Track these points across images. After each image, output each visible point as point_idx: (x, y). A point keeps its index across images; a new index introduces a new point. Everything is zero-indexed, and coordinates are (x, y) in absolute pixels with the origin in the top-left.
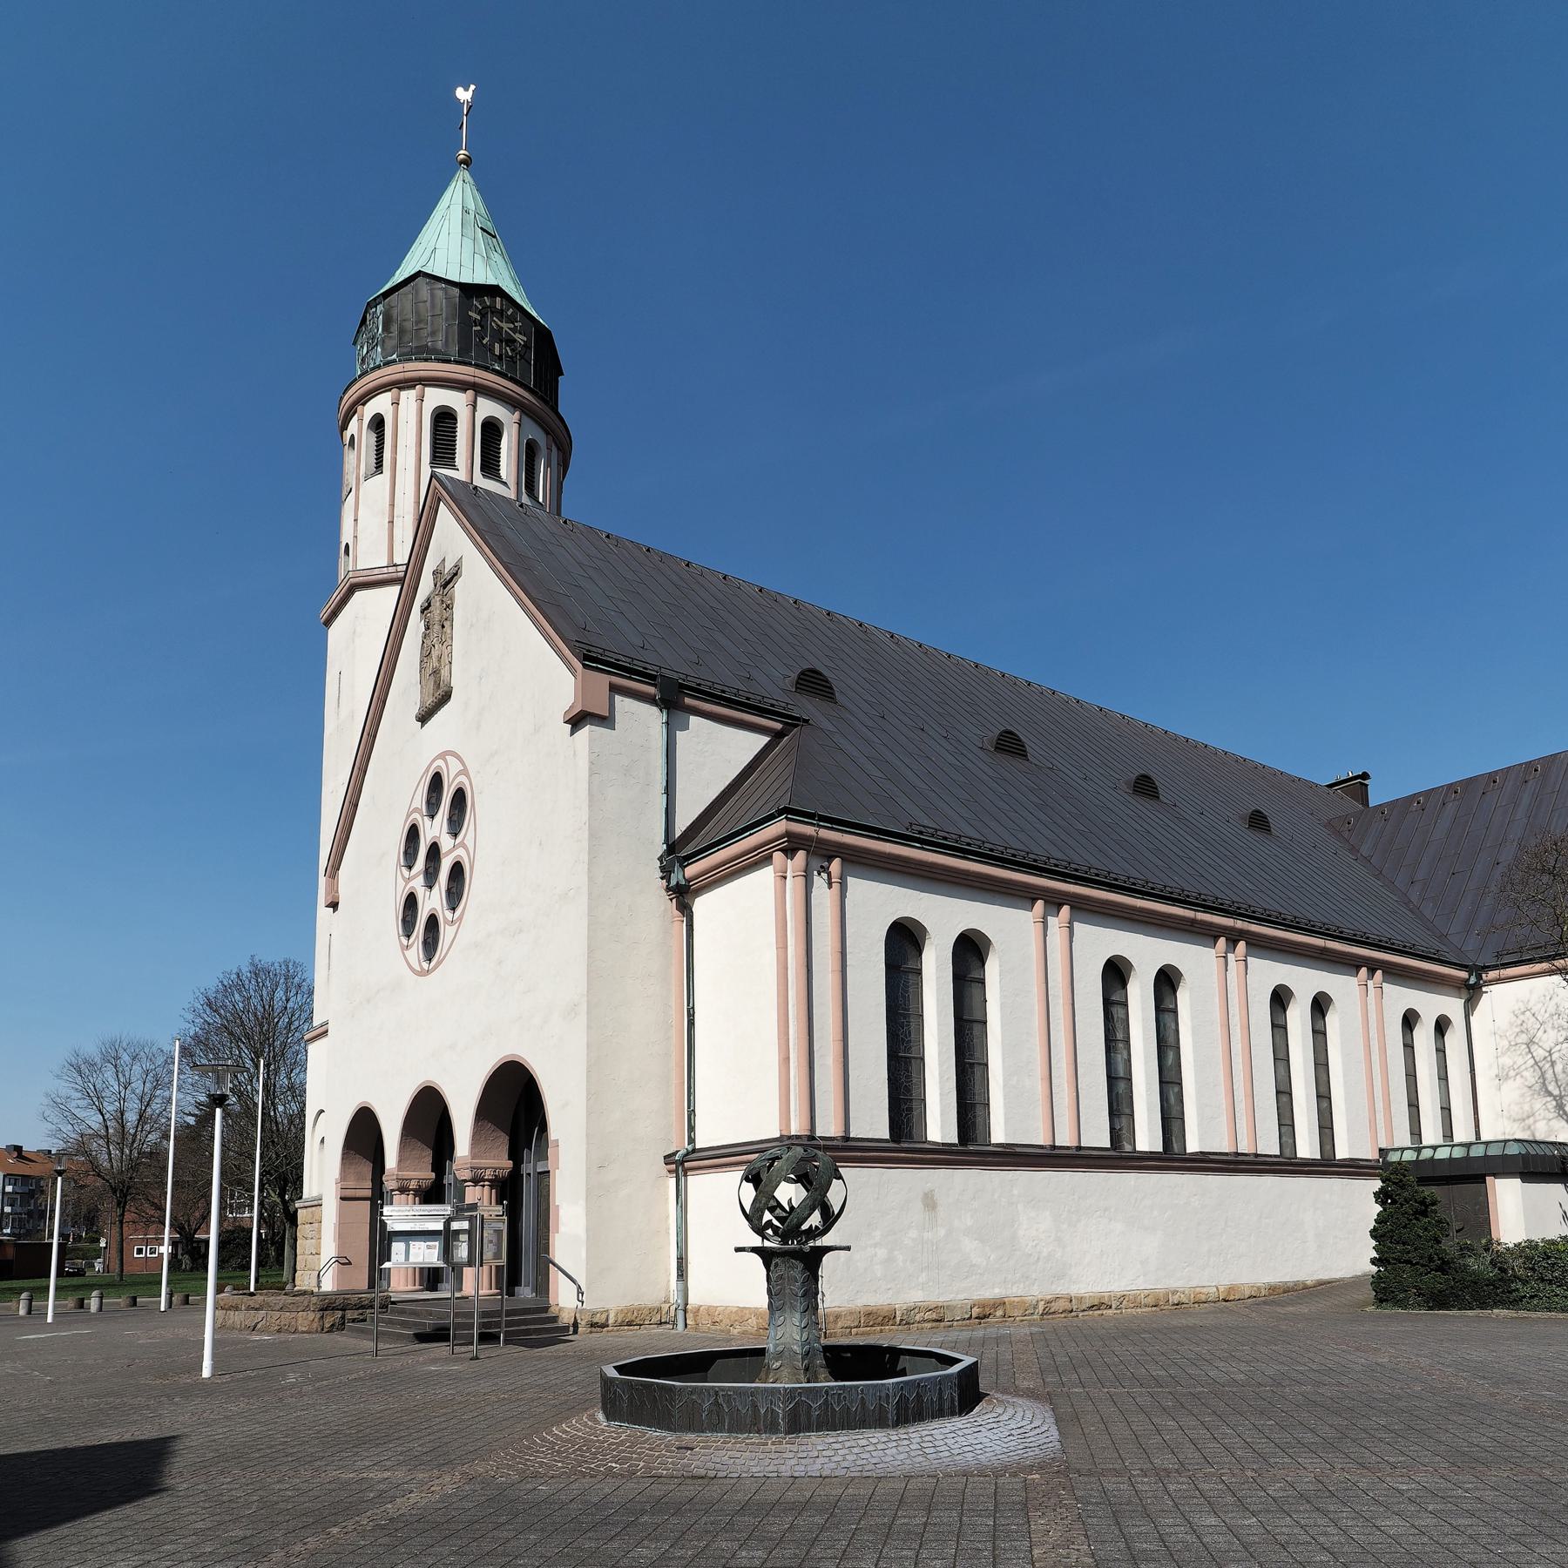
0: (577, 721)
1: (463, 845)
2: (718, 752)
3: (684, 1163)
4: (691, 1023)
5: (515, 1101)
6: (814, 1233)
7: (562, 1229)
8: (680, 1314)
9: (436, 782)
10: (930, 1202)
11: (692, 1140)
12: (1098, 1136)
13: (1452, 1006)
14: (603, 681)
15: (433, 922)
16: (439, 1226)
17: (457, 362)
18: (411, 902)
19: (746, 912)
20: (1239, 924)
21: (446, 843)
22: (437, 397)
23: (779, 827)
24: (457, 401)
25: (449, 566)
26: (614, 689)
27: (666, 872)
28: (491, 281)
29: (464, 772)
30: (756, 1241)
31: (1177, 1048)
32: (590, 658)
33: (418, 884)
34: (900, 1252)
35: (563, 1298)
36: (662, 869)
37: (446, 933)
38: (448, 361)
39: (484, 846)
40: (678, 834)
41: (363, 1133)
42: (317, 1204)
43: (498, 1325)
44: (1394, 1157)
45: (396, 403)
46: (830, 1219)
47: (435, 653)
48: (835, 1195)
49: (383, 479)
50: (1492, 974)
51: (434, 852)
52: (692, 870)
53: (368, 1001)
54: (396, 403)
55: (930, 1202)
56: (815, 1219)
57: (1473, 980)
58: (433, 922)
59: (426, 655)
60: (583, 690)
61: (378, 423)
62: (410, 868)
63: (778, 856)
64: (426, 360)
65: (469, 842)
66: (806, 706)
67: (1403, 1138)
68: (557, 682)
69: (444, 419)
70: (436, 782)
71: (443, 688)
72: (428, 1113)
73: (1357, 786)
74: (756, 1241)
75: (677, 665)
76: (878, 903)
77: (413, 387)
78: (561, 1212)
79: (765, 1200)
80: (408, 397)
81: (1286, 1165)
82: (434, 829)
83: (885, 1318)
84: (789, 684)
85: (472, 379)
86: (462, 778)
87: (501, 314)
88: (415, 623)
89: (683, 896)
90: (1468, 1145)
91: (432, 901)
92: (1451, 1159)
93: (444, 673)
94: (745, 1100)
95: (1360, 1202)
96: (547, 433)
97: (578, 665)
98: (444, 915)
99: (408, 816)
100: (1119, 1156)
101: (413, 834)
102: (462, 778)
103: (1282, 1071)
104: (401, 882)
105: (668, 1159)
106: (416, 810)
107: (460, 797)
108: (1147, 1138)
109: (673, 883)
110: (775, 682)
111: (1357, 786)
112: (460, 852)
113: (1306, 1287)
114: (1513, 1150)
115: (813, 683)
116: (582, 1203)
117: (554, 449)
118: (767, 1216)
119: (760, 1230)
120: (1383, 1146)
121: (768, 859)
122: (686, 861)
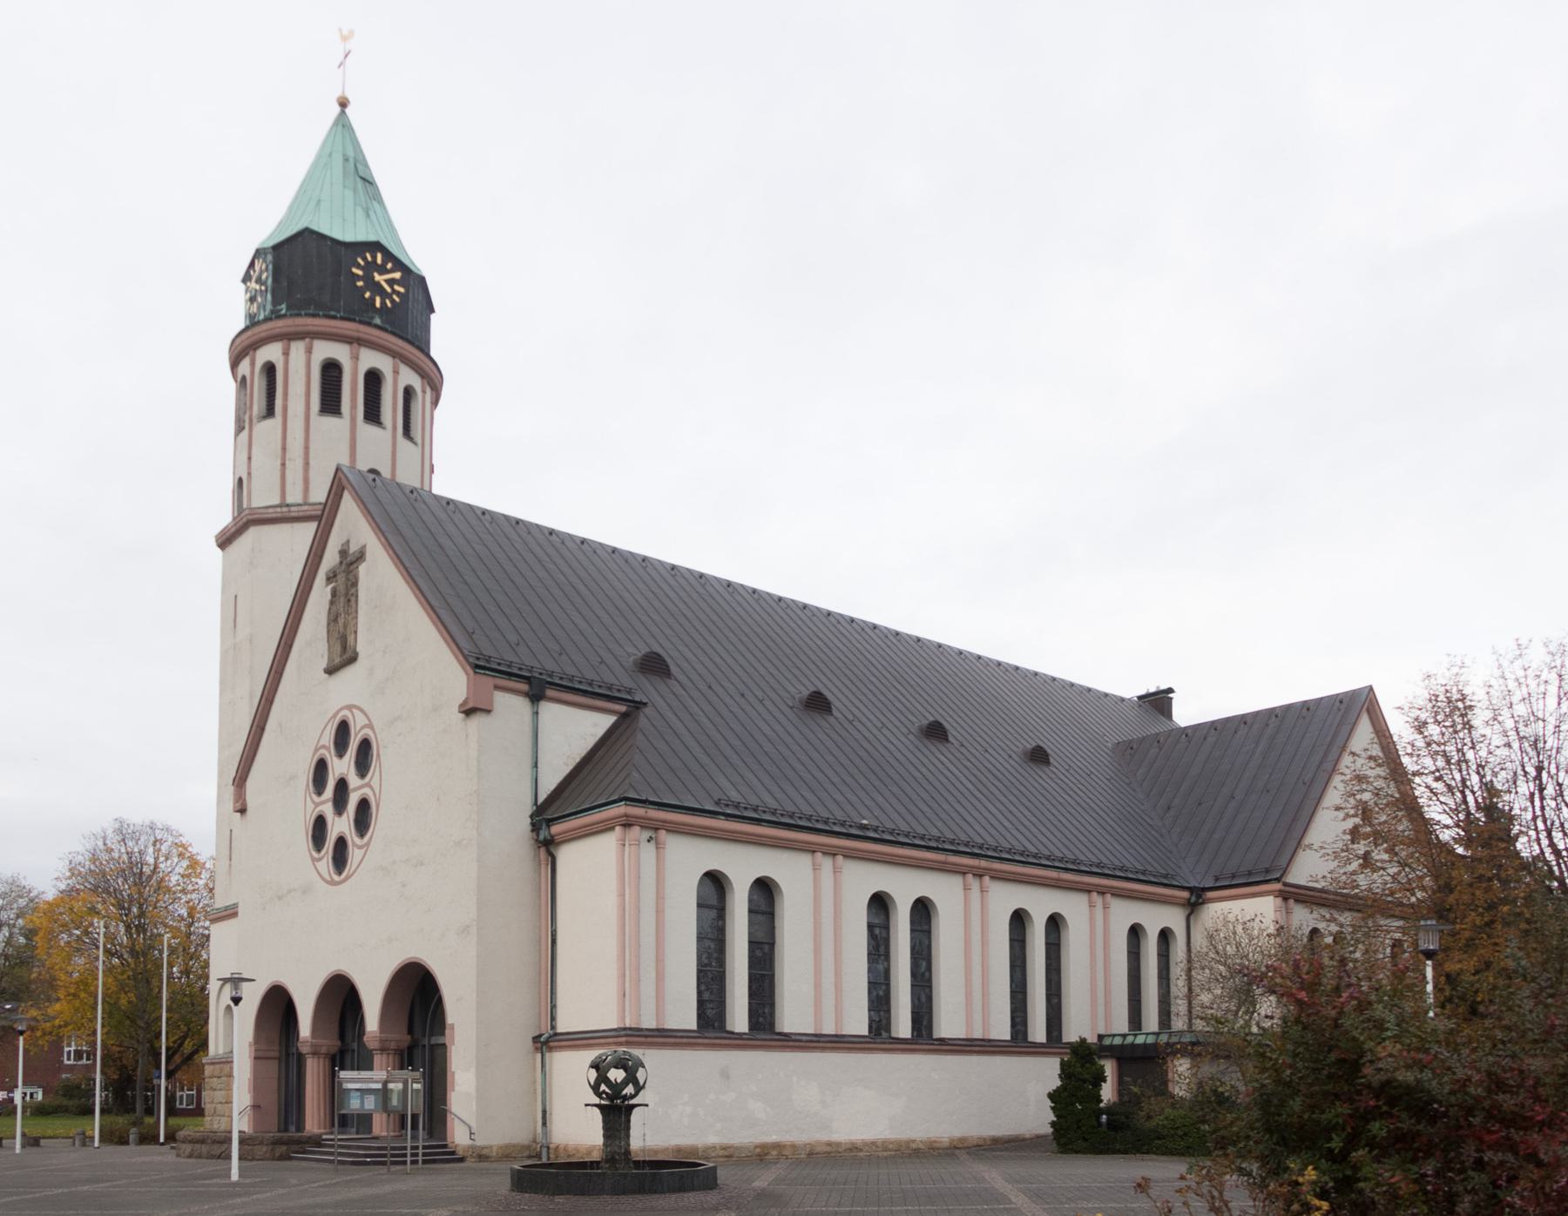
0: (469, 712)
1: (368, 785)
2: (573, 731)
3: (547, 1041)
4: (554, 942)
5: (417, 991)
6: (633, 1097)
9: (343, 730)
10: (725, 1075)
11: (553, 1027)
12: (857, 1022)
13: (1173, 918)
14: (487, 681)
15: (341, 843)
16: (379, 1086)
17: (342, 318)
18: (320, 824)
19: (592, 864)
20: (983, 863)
21: (353, 781)
22: (325, 350)
23: (620, 809)
24: (340, 352)
25: (353, 548)
26: (497, 687)
27: (535, 827)
28: (372, 238)
29: (370, 726)
30: (597, 1100)
32: (479, 665)
33: (328, 810)
34: (690, 1105)
35: (459, 1136)
36: (533, 824)
39: (388, 784)
41: (278, 1004)
42: (227, 1061)
44: (1107, 1042)
45: (286, 353)
46: (639, 1089)
47: (341, 621)
48: (640, 1075)
49: (274, 424)
50: (1210, 894)
51: (342, 785)
52: (555, 829)
53: (280, 898)
54: (286, 353)
55: (725, 1075)
56: (629, 1090)
57: (1193, 899)
58: (341, 843)
59: (333, 619)
61: (270, 369)
62: (319, 794)
64: (314, 316)
65: (375, 783)
66: (647, 689)
67: (1121, 1024)
68: (455, 680)
69: (331, 371)
70: (343, 730)
71: (349, 654)
72: (341, 996)
73: (1159, 702)
74: (597, 1100)
75: (545, 662)
76: (689, 859)
77: (303, 338)
78: (457, 1076)
79: (603, 1078)
80: (297, 348)
83: (694, 1151)
84: (629, 662)
85: (355, 334)
88: (320, 594)
89: (547, 846)
92: (1145, 1045)
93: (351, 639)
94: (589, 1002)
95: (1046, 1073)
96: (423, 377)
97: (471, 671)
98: (352, 837)
99: (316, 750)
100: (879, 1034)
101: (321, 768)
102: (368, 731)
103: (1018, 974)
104: (310, 806)
106: (323, 747)
107: (365, 745)
109: (541, 837)
110: (621, 676)
111: (1159, 702)
112: (367, 791)
113: (1024, 1140)
115: (653, 665)
117: (428, 390)
118: (603, 1087)
119: (598, 1094)
120: (1102, 1032)
121: (612, 829)
122: (550, 822)
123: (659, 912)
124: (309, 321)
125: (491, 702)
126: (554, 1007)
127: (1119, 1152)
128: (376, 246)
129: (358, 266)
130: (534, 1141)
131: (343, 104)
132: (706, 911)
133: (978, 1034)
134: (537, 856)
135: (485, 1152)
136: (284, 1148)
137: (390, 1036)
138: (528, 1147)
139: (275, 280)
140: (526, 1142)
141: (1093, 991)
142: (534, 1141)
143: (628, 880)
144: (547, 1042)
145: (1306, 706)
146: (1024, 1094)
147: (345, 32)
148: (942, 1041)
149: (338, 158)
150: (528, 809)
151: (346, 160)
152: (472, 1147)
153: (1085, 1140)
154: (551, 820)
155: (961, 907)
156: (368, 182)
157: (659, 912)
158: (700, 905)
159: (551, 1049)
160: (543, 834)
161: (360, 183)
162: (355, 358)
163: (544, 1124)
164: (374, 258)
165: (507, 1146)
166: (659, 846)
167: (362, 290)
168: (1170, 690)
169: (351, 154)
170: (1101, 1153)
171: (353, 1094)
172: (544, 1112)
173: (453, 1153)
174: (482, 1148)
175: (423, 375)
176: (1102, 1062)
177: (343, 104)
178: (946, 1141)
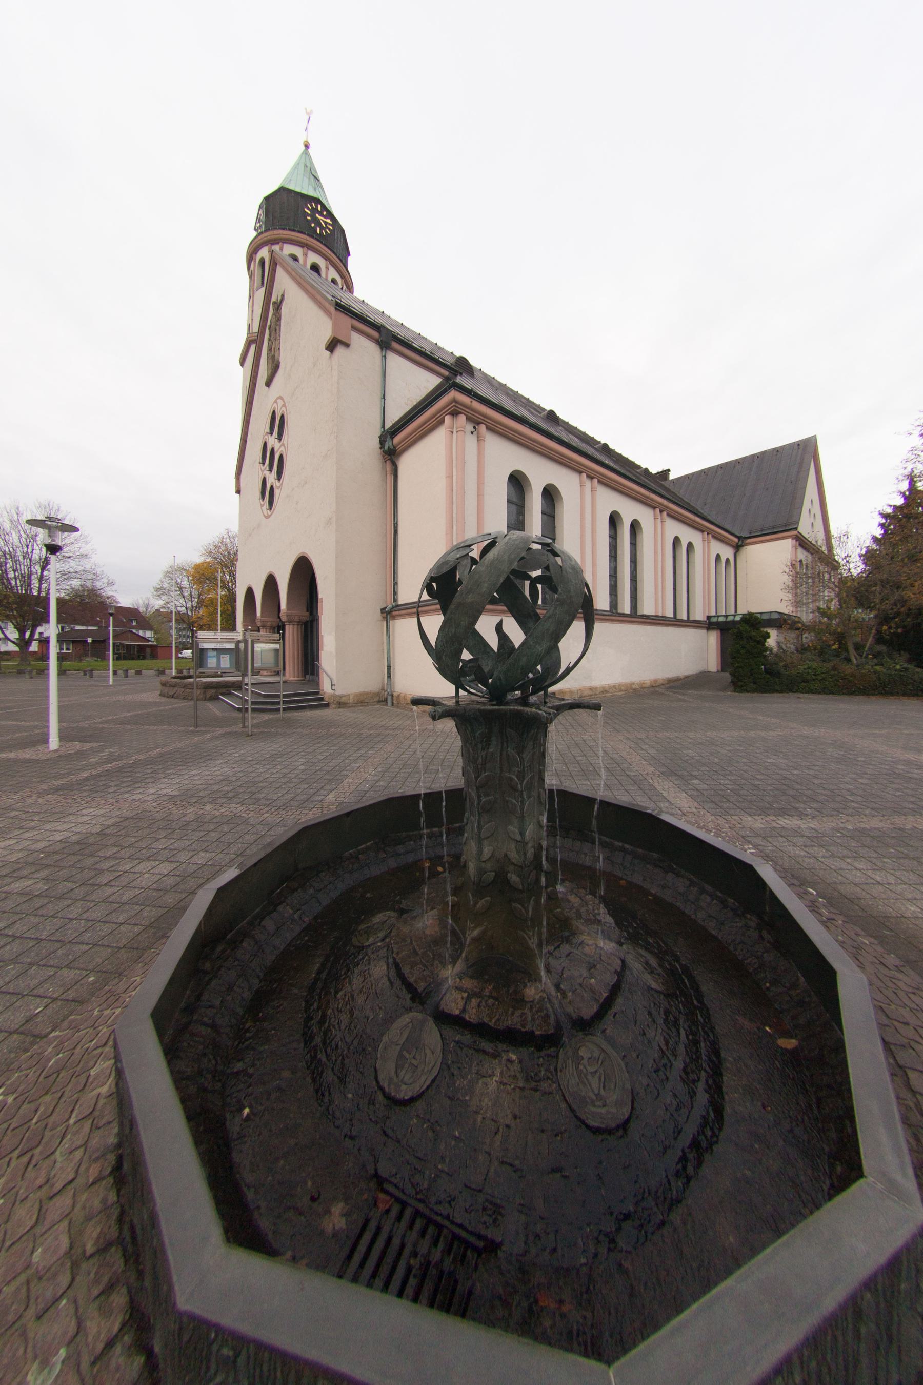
1: (283, 445)
3: (391, 612)
4: (396, 532)
7: (325, 648)
8: (389, 697)
11: (395, 600)
20: (665, 502)
26: (354, 328)
27: (382, 442)
29: (284, 405)
31: (631, 561)
35: (326, 687)
37: (277, 493)
38: (294, 231)
39: (292, 447)
40: (433, 644)
43: (278, 703)
44: (714, 620)
59: (270, 350)
60: (335, 327)
63: (448, 419)
65: (285, 442)
74: (443, 689)
81: (675, 622)
82: (272, 441)
86: (284, 409)
87: (321, 214)
90: (726, 616)
91: (271, 479)
93: (277, 355)
98: (277, 484)
105: (383, 610)
108: (625, 607)
109: (386, 448)
112: (282, 449)
114: (776, 616)
116: (334, 633)
121: (441, 422)
123: (480, 495)
124: (281, 232)
125: (350, 338)
126: (395, 584)
127: (777, 691)
128: (318, 201)
129: (308, 208)
130: (383, 689)
131: (307, 146)
132: (512, 505)
133: (660, 614)
134: (384, 469)
135: (343, 699)
136: (213, 691)
137: (294, 612)
138: (378, 694)
139: (267, 216)
140: (377, 691)
141: (704, 592)
142: (383, 689)
143: (455, 464)
144: (390, 612)
145: (776, 451)
146: (699, 652)
147: (308, 111)
148: (643, 616)
149: (302, 167)
150: (378, 432)
151: (306, 166)
152: (334, 696)
153: (755, 683)
154: (393, 444)
155: (653, 529)
156: (317, 179)
157: (480, 495)
158: (509, 501)
159: (393, 618)
160: (388, 444)
161: (312, 177)
162: (305, 255)
163: (389, 677)
164: (317, 207)
165: (361, 694)
166: (480, 439)
167: (309, 222)
168: (669, 470)
169: (309, 165)
170: (765, 692)
171: (210, 654)
172: (389, 667)
173: (322, 699)
174: (341, 696)
175: (342, 277)
176: (769, 630)
177: (307, 146)
178: (648, 684)
